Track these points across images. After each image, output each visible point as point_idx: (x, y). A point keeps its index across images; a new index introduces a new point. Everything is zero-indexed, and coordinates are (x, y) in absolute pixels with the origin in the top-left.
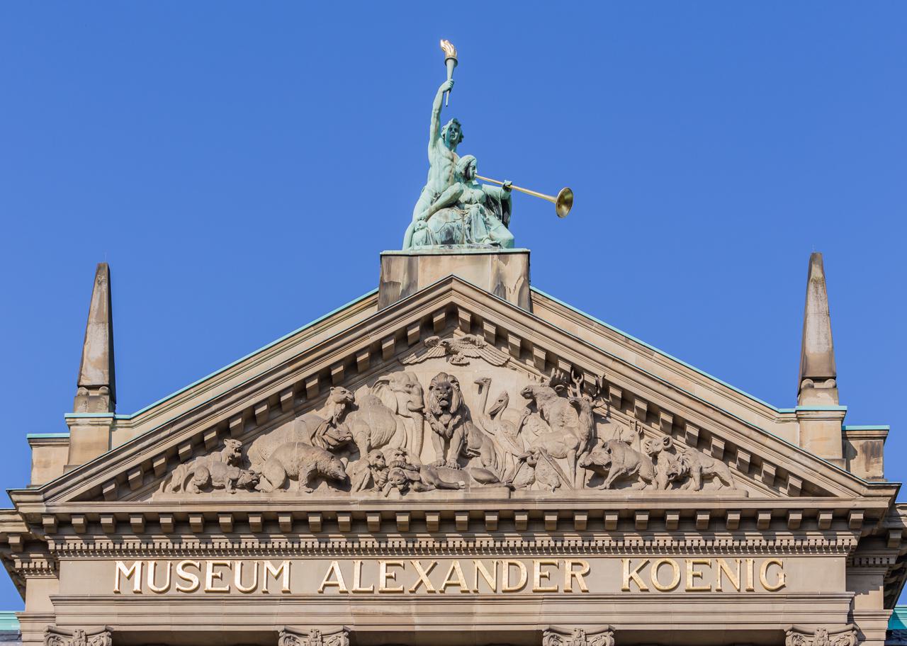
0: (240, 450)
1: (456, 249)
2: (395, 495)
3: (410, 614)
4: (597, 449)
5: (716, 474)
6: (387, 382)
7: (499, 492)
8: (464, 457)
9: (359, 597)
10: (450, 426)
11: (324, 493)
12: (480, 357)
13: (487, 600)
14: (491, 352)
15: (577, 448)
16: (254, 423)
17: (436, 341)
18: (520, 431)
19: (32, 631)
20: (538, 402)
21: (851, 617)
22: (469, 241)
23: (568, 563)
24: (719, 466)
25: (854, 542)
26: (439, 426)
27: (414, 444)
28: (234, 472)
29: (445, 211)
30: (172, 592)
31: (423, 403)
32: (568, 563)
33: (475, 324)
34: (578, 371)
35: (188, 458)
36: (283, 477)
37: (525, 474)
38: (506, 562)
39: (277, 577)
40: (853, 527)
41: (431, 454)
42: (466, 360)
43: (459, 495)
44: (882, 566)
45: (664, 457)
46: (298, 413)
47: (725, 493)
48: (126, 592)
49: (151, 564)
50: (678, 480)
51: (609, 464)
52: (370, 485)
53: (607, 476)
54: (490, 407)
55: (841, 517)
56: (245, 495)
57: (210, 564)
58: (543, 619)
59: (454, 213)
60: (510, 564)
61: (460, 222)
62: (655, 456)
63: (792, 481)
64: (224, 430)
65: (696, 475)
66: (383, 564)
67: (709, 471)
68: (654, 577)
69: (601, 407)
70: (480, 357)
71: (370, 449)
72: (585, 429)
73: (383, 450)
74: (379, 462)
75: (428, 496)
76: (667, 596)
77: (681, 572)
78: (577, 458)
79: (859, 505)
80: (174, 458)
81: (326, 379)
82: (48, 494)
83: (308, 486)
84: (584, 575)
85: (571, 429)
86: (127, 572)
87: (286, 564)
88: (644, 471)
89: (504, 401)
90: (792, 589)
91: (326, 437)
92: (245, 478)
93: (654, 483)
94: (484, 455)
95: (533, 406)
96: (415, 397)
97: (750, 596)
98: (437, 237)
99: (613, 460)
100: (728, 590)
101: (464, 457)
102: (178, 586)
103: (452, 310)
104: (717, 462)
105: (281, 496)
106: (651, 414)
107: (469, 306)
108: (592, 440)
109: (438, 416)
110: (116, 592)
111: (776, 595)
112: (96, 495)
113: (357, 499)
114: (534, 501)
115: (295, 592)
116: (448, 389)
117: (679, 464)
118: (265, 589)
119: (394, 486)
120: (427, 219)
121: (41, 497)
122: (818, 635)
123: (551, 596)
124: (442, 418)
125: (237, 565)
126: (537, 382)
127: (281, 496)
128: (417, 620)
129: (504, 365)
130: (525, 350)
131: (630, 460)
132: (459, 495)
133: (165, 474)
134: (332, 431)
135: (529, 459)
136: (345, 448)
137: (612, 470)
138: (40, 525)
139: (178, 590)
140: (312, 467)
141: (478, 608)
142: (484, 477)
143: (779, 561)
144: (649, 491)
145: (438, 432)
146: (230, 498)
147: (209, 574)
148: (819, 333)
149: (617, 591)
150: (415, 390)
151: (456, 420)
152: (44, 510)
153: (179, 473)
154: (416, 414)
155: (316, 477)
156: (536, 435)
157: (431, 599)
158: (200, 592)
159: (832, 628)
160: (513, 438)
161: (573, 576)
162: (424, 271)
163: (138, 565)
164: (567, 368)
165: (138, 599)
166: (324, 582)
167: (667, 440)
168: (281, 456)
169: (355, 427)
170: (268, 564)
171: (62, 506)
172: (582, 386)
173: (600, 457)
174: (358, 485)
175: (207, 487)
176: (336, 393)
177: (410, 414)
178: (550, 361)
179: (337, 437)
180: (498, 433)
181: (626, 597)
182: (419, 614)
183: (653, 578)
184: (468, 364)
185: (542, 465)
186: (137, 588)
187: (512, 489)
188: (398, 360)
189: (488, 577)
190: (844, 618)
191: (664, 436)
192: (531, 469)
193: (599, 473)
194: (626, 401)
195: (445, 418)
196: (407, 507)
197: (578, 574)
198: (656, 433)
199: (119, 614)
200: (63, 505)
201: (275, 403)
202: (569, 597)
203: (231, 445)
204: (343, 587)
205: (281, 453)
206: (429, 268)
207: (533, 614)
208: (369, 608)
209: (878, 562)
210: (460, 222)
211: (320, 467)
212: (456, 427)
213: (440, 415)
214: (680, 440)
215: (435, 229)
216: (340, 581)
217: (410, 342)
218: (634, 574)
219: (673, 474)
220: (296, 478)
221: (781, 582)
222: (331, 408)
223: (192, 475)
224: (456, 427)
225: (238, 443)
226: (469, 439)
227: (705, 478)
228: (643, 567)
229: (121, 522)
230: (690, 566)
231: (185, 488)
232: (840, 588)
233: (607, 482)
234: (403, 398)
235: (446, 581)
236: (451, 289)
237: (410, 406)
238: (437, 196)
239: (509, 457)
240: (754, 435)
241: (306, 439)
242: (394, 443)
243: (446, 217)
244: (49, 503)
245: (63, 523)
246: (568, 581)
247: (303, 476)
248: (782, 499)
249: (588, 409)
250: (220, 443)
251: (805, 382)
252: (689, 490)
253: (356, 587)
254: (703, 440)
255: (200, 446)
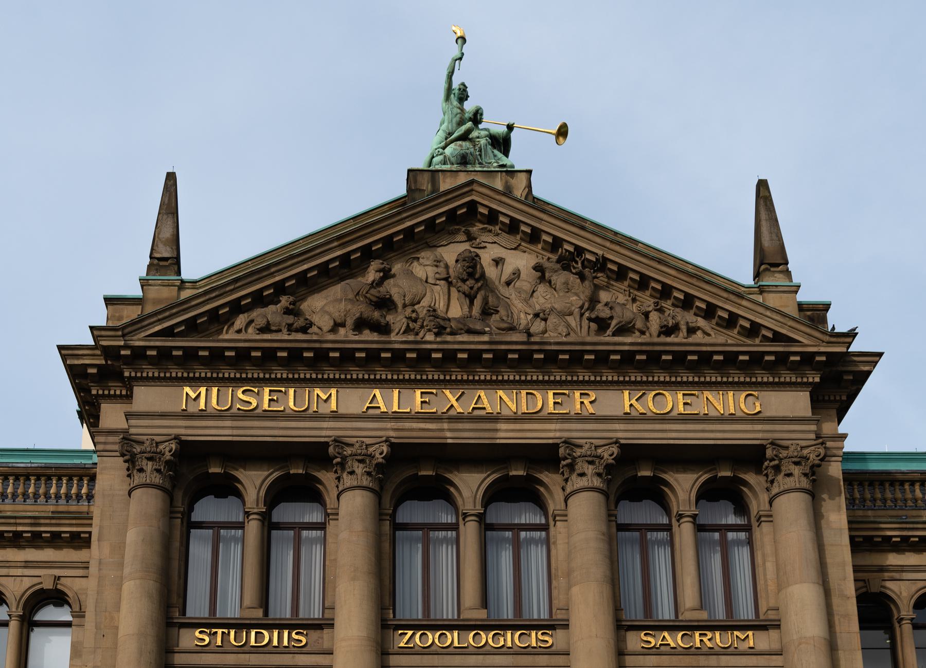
0: (293, 303)
1: (470, 168)
2: (430, 337)
3: (442, 430)
4: (599, 306)
5: (699, 328)
6: (418, 258)
7: (515, 337)
8: (487, 312)
9: (397, 417)
10: (475, 288)
11: (368, 335)
12: (495, 243)
13: (508, 420)
14: (505, 239)
15: (581, 307)
16: (307, 284)
17: (459, 230)
18: (532, 295)
19: (105, 443)
20: (547, 275)
21: (818, 437)
22: (480, 163)
23: (577, 394)
24: (701, 322)
25: (817, 380)
26: (465, 288)
27: (442, 304)
28: (290, 319)
29: (459, 143)
30: (234, 410)
31: (448, 273)
32: (577, 394)
33: (492, 217)
34: (580, 250)
35: (248, 309)
36: (332, 323)
37: (537, 327)
38: (524, 392)
39: (326, 401)
40: (818, 367)
41: (456, 310)
42: (483, 245)
43: (486, 338)
44: (835, 401)
45: (654, 316)
46: (342, 279)
47: (707, 340)
48: (192, 409)
49: (215, 390)
50: (668, 331)
51: (611, 318)
52: (408, 330)
53: (608, 328)
54: (504, 278)
55: (808, 359)
56: (300, 336)
57: (267, 390)
58: (558, 434)
59: (466, 144)
60: (527, 393)
61: (472, 150)
62: (646, 315)
63: (764, 332)
64: (280, 289)
65: (684, 328)
66: (418, 392)
67: (693, 325)
68: (651, 404)
69: (602, 278)
70: (495, 243)
71: (405, 306)
72: (588, 292)
73: (416, 307)
74: (414, 315)
75: (460, 338)
76: (664, 418)
77: (674, 401)
78: (582, 315)
79: (822, 349)
80: (237, 308)
81: (367, 254)
82: (126, 331)
83: (354, 330)
84: (591, 402)
85: (576, 294)
86: (193, 395)
87: (333, 391)
88: (639, 324)
89: (517, 274)
90: (768, 413)
91: (368, 295)
92: (300, 322)
93: (647, 334)
94: (503, 312)
95: (542, 279)
96: (441, 270)
97: (732, 419)
98: (453, 159)
99: (614, 314)
100: (713, 413)
101: (487, 312)
102: (238, 406)
103: (472, 206)
104: (699, 319)
105: (331, 337)
106: (643, 283)
107: (486, 203)
108: (593, 301)
109: (464, 281)
110: (183, 410)
111: (755, 419)
112: (168, 333)
113: (397, 339)
114: (550, 344)
115: (341, 411)
116: (471, 265)
117: (670, 319)
118: (315, 409)
119: (429, 330)
120: (444, 148)
121: (120, 333)
122: (792, 448)
123: (565, 418)
124: (468, 283)
125: (291, 391)
126: (549, 259)
127: (331, 337)
128: (448, 434)
129: (515, 249)
130: (534, 236)
131: (628, 315)
132: (486, 338)
133: (228, 320)
134: (373, 291)
135: (541, 315)
136: (385, 304)
137: (614, 323)
138: (119, 357)
139: (239, 409)
140: (358, 315)
141: (502, 426)
142: (504, 325)
143: (755, 393)
144: (645, 339)
145: (464, 293)
146: (286, 337)
147: (266, 398)
148: (771, 233)
149: (620, 413)
150: (442, 264)
151: (480, 284)
152: (122, 343)
153: (240, 321)
154: (443, 282)
155: (361, 324)
156: (543, 298)
157: (460, 418)
158: (259, 411)
159: (804, 443)
160: (526, 301)
161: (582, 403)
162: (444, 182)
163: (203, 390)
164: (571, 249)
165: (202, 415)
166: (368, 405)
167: (656, 304)
168: (330, 309)
169: (395, 289)
170: (317, 391)
171: (138, 341)
172: (583, 263)
173: (604, 313)
174: (397, 330)
175: (266, 329)
176: (375, 265)
177: (438, 282)
178: (557, 243)
179: (377, 295)
180: (513, 296)
181: (627, 418)
182: (450, 430)
183: (650, 404)
184: (485, 247)
185: (553, 320)
186: (202, 406)
187: (530, 335)
188: (426, 243)
189: (510, 404)
190: (813, 436)
191: (653, 300)
192: (543, 322)
193: (602, 324)
194: (622, 273)
195: (470, 282)
196: (440, 347)
197: (586, 402)
198: (647, 300)
199: (186, 427)
200: (139, 340)
201: (323, 269)
202: (580, 418)
203: (285, 301)
204: (383, 409)
205: (326, 308)
206: (448, 180)
207: (550, 431)
208: (407, 425)
209: (832, 398)
210: (472, 150)
211: (365, 316)
212: (479, 289)
213: (467, 280)
214: (667, 304)
215: (451, 154)
216: (381, 405)
217: (437, 229)
218: (633, 401)
219: (665, 326)
220: (343, 325)
221: (758, 409)
222: (372, 275)
223: (252, 321)
224: (479, 289)
225: (292, 299)
226: (490, 299)
227: (692, 331)
228: (640, 397)
229: (190, 355)
230: (680, 396)
231: (246, 331)
232: (808, 413)
233: (609, 332)
234: (431, 271)
235: (473, 406)
236: (472, 190)
237: (437, 276)
238: (450, 134)
239: (522, 315)
240: (732, 297)
241: (351, 296)
242: (425, 302)
243: (461, 146)
244: (127, 338)
245: (139, 354)
246: (578, 406)
247: (350, 322)
248: (756, 345)
249: (591, 279)
250: (276, 300)
251: (763, 267)
252: (678, 338)
253: (395, 408)
254: (687, 302)
255: (259, 300)
